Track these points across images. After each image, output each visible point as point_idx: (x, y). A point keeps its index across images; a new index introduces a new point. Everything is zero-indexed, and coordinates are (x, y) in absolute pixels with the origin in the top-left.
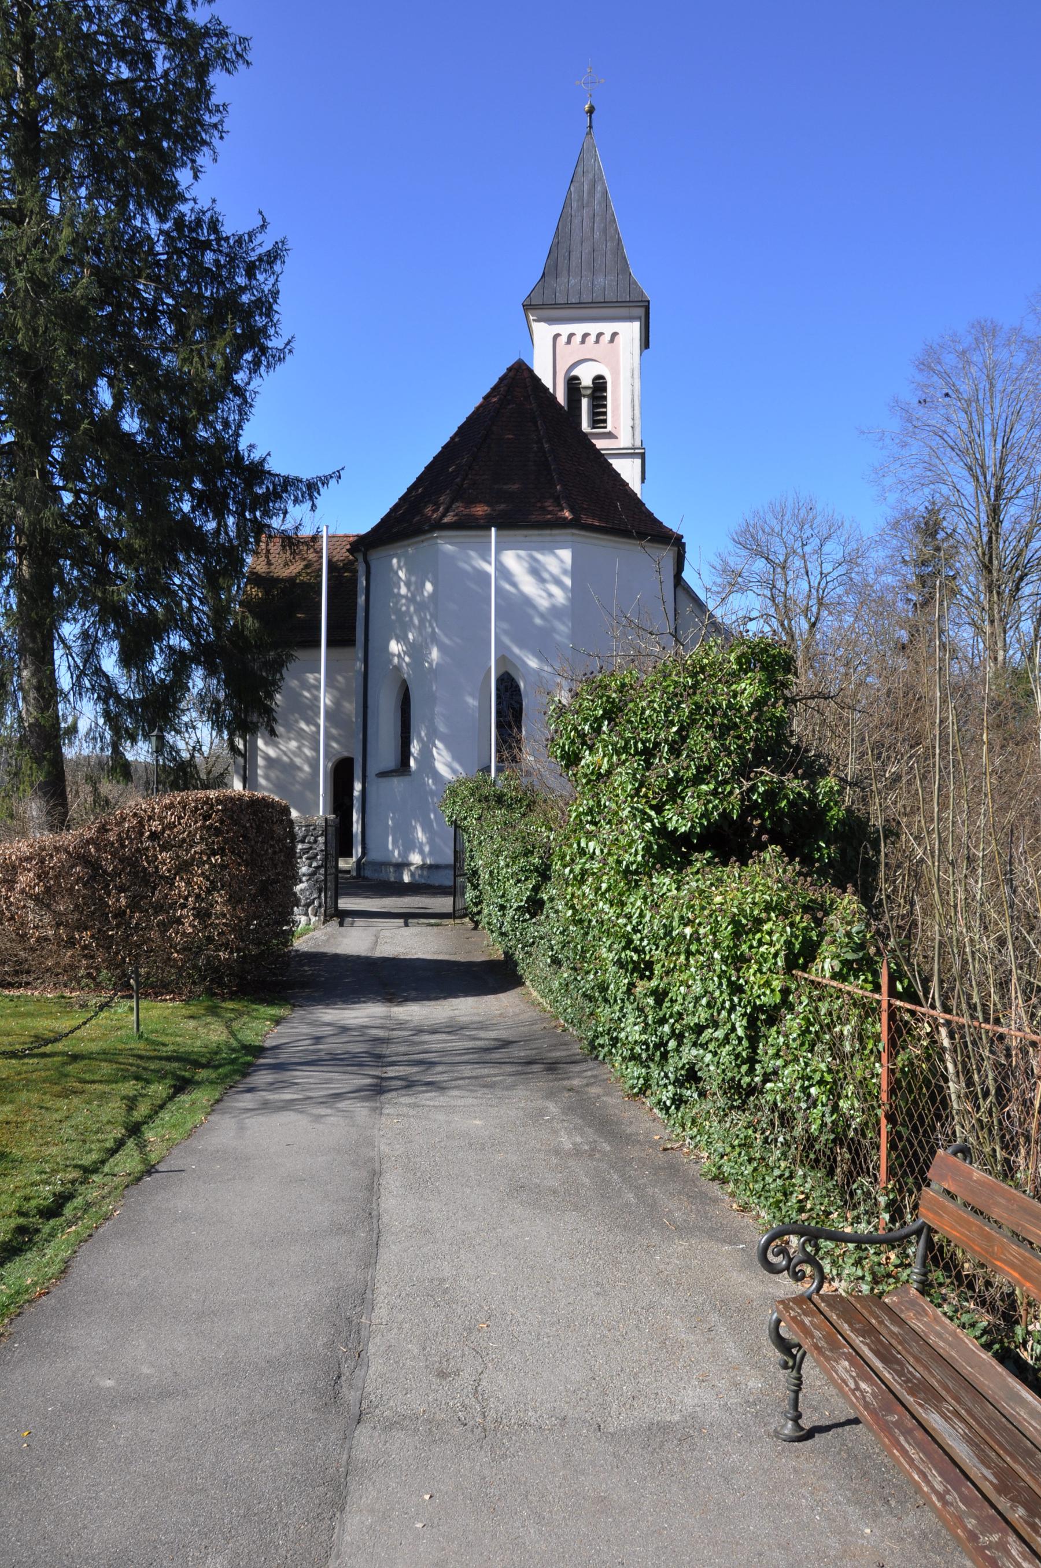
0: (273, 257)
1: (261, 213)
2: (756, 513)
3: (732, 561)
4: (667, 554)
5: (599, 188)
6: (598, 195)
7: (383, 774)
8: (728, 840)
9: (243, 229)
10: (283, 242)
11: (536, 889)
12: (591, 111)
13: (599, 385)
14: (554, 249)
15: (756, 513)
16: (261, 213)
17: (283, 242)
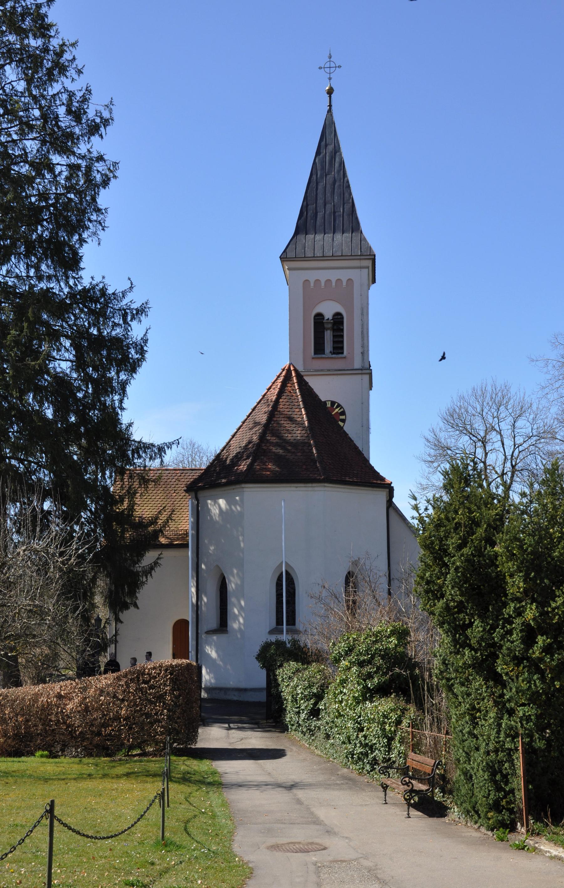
0: (141, 311)
1: (129, 279)
2: (462, 398)
3: (442, 436)
4: (382, 495)
5: (337, 159)
6: (337, 165)
7: (208, 632)
8: (382, 691)
9: (120, 290)
10: (146, 303)
11: (316, 704)
12: (330, 92)
13: (338, 319)
14: (304, 210)
15: (462, 398)
16: (129, 279)
17: (146, 303)
